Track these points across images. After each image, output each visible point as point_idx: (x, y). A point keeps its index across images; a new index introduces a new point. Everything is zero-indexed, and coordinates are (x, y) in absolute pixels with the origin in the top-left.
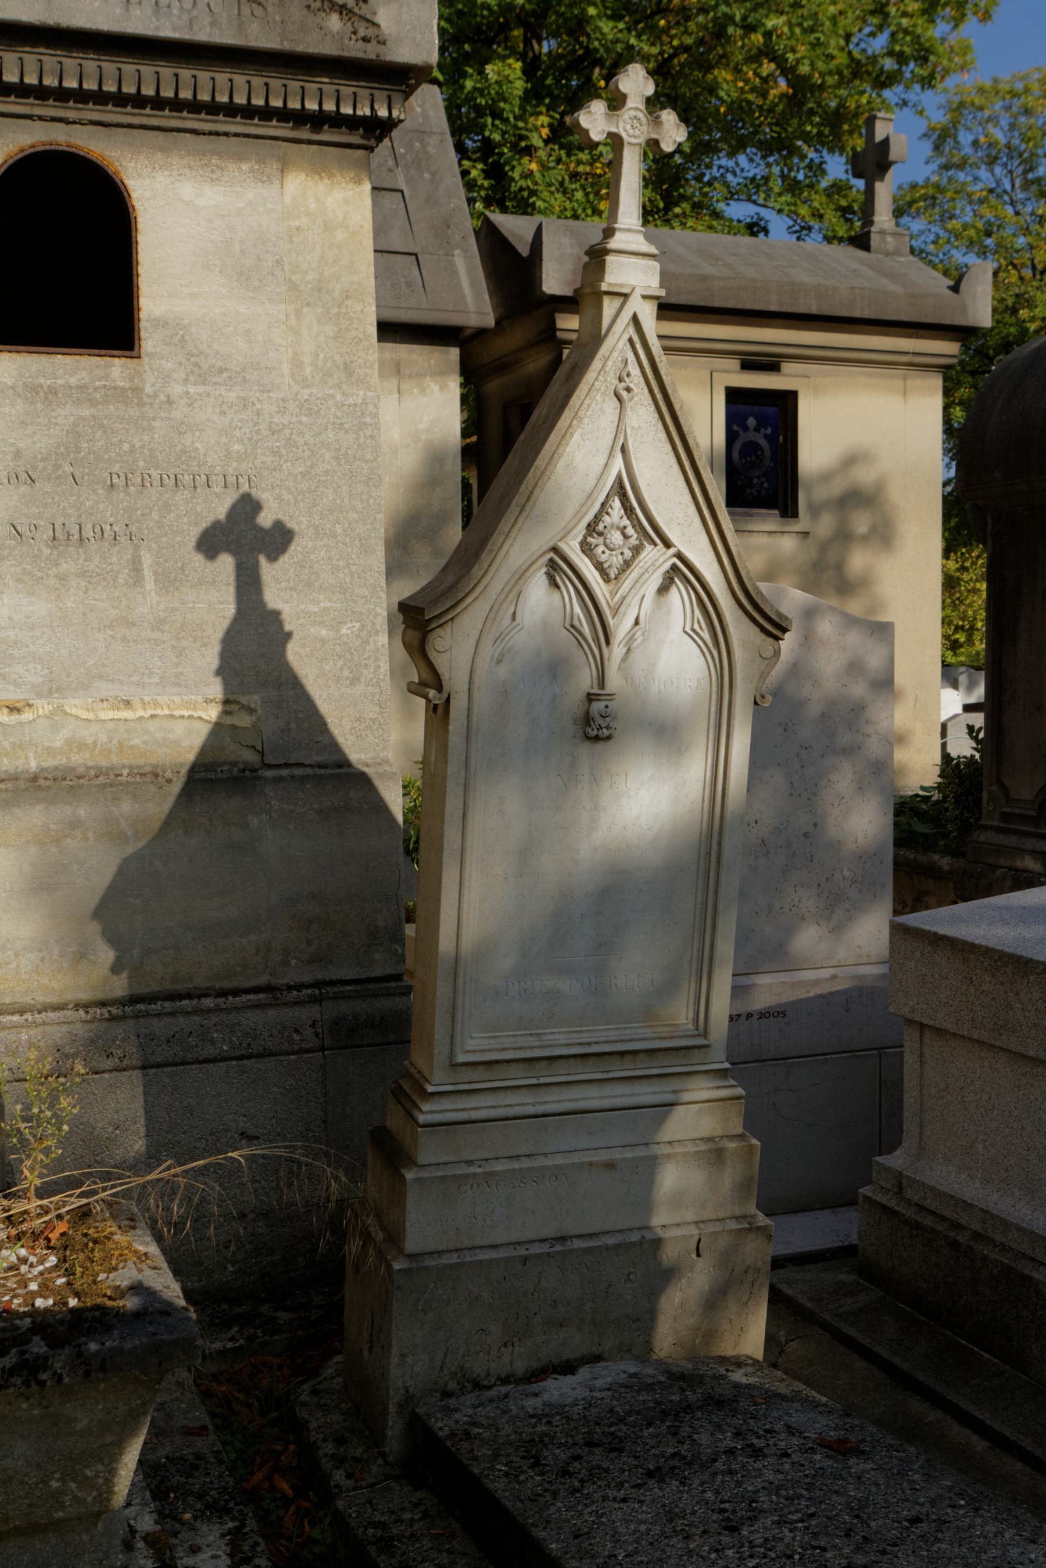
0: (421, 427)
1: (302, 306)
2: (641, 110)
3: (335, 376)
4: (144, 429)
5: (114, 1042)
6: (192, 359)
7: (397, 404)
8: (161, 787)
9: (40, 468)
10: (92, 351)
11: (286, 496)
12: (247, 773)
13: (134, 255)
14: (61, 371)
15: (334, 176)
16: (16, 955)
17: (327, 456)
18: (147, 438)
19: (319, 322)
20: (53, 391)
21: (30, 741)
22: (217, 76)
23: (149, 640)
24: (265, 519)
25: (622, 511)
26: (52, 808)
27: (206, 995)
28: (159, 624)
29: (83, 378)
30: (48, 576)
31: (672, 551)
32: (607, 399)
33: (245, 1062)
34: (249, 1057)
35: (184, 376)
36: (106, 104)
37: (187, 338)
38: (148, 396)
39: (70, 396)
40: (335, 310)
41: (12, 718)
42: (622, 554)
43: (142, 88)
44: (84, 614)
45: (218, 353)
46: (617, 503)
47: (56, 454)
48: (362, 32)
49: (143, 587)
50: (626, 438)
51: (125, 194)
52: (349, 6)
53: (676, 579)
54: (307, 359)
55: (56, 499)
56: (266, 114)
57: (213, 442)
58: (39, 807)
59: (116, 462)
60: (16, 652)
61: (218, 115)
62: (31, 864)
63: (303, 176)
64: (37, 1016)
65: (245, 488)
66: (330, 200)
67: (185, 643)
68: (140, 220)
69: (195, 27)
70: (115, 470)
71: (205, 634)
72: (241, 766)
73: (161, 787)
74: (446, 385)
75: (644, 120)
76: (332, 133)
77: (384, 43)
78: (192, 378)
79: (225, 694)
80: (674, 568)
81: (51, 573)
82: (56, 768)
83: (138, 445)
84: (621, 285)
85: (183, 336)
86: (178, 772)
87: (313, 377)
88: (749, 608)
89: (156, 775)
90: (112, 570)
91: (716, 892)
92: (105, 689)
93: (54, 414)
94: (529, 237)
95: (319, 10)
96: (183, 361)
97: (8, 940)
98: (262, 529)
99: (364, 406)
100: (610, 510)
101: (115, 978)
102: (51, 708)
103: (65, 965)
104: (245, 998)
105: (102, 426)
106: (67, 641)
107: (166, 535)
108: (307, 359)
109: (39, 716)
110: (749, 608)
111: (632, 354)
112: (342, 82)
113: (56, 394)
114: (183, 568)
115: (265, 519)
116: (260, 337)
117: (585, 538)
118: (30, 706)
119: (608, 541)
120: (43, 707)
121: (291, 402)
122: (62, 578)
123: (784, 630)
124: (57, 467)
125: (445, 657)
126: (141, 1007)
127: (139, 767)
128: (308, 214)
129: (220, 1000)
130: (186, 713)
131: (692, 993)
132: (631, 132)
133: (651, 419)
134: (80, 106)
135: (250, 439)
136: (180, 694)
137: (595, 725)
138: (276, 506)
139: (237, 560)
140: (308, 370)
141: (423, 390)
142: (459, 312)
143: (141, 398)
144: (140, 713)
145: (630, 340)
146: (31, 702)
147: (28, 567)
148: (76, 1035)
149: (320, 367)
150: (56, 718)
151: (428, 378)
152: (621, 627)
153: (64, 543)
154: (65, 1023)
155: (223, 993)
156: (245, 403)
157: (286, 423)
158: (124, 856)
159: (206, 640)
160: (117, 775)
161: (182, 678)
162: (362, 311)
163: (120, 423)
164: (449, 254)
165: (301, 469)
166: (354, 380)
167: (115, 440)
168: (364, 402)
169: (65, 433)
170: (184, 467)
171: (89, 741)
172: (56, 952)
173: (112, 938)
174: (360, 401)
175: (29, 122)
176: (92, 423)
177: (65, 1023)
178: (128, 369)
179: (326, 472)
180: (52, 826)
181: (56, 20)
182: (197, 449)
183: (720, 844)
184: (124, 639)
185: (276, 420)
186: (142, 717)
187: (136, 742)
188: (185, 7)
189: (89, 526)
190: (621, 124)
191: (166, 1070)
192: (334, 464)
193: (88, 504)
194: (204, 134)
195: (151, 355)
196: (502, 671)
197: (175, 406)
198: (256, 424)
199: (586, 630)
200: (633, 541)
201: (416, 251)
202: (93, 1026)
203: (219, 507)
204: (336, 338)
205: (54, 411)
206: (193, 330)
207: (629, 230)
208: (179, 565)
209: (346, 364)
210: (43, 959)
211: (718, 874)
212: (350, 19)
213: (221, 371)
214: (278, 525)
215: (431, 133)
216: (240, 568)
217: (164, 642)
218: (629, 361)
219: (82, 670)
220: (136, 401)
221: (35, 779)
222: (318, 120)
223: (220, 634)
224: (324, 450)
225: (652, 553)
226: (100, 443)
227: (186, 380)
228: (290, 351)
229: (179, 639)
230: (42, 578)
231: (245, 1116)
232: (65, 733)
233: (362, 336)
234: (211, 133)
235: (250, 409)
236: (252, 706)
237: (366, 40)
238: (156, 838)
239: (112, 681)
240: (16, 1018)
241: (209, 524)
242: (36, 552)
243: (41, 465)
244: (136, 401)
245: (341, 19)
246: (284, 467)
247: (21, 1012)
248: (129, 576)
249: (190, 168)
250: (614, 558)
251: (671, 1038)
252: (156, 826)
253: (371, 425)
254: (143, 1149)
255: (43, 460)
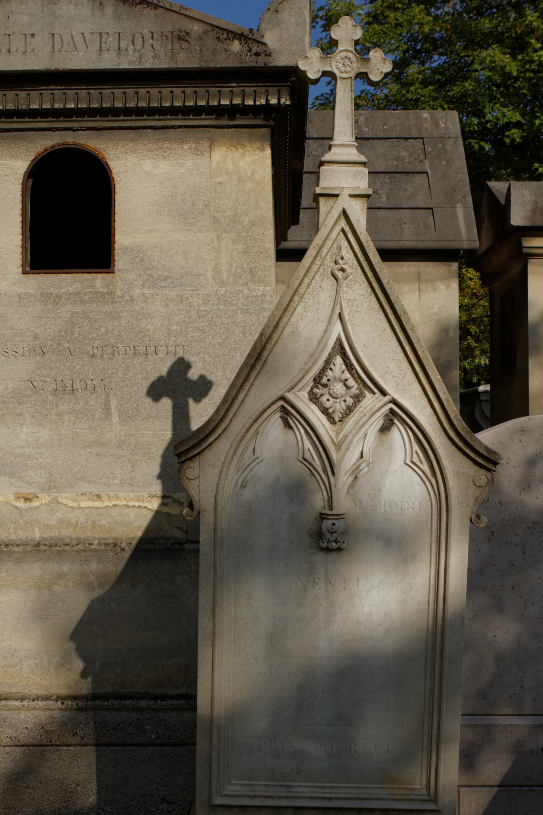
0: (433, 311)
1: (222, 233)
2: (350, 52)
3: (243, 278)
4: (115, 318)
5: (79, 725)
6: (148, 272)
7: (418, 298)
8: (117, 554)
9: (49, 345)
10: (83, 270)
11: (208, 359)
12: (176, 545)
13: (113, 209)
14: (64, 284)
15: (246, 147)
16: (21, 661)
17: (237, 332)
18: (116, 324)
19: (233, 243)
20: (59, 296)
21: (36, 520)
22: (163, 90)
23: (113, 455)
24: (193, 374)
25: (344, 367)
26: (46, 564)
27: (143, 698)
28: (121, 444)
29: (78, 288)
30: (51, 413)
31: (387, 398)
32: (325, 279)
33: (166, 748)
34: (169, 745)
35: (142, 283)
36: (96, 116)
37: (144, 258)
38: (118, 297)
39: (69, 299)
40: (244, 234)
41: (26, 505)
42: (345, 401)
43: (115, 103)
44: (73, 438)
45: (164, 267)
46: (339, 360)
47: (59, 336)
48: (255, 50)
49: (111, 420)
50: (341, 309)
51: (109, 171)
52: (245, 34)
53: (396, 421)
54: (224, 268)
55: (58, 365)
56: (197, 111)
57: (159, 324)
58: (38, 564)
59: (97, 340)
60: (29, 462)
61: (166, 115)
62: (32, 601)
63: (224, 149)
64: (31, 703)
65: (180, 354)
66: (242, 163)
67: (137, 458)
68: (117, 186)
69: (143, 60)
70: (95, 345)
71: (151, 451)
72: (173, 541)
73: (117, 554)
74: (449, 286)
75: (354, 58)
76: (243, 119)
77: (270, 55)
78: (147, 284)
79: (163, 491)
80: (392, 411)
81: (53, 411)
82: (52, 538)
83: (111, 328)
84: (333, 188)
85: (142, 258)
86: (130, 544)
87: (228, 279)
88: (460, 444)
89: (115, 545)
90: (91, 410)
91: (441, 678)
92: (84, 487)
93: (58, 311)
94: (505, 191)
95: (225, 39)
96: (142, 273)
97: (16, 650)
98: (191, 381)
99: (263, 297)
100: (332, 366)
101: (83, 681)
102: (50, 499)
103: (51, 670)
104: (169, 702)
105: (88, 317)
106: (62, 455)
107: (127, 386)
108: (224, 268)
109: (42, 504)
110: (460, 444)
111: (346, 242)
112: (245, 85)
113: (61, 299)
114: (137, 408)
115: (193, 374)
116: (193, 255)
117: (312, 389)
118: (37, 497)
119: (331, 391)
120: (45, 498)
121: (213, 296)
122: (60, 415)
123: (495, 464)
124: (59, 344)
125: (195, 483)
126: (98, 702)
127: (105, 539)
128: (227, 173)
129: (152, 702)
130: (137, 504)
131: (425, 763)
132: (343, 69)
133: (365, 292)
134: (80, 119)
135: (184, 322)
136: (133, 491)
137: (327, 537)
138: (200, 365)
139: (173, 402)
140: (225, 275)
141: (435, 289)
142: (456, 240)
143: (114, 298)
144: (107, 503)
145: (343, 230)
146: (38, 495)
147: (39, 408)
148: (55, 718)
149: (233, 272)
150: (53, 505)
151: (438, 281)
152: (347, 461)
153: (62, 392)
154: (48, 709)
155: (155, 698)
156: (181, 299)
157: (209, 310)
158: (92, 599)
159: (151, 455)
160: (90, 544)
161: (135, 480)
162: (263, 234)
163: (100, 315)
164: (453, 207)
165: (219, 341)
166: (256, 279)
167: (96, 326)
168: (264, 294)
169: (65, 322)
170: (140, 341)
171: (73, 521)
172: (45, 660)
173: (82, 653)
174: (261, 293)
175: (51, 132)
176: (82, 315)
177: (48, 709)
178: (106, 280)
179: (236, 342)
180: (46, 577)
181: (56, 67)
182: (149, 330)
183: (442, 640)
184: (98, 455)
185: (202, 309)
186: (107, 506)
187: (104, 522)
188: (137, 49)
189: (78, 381)
190: (334, 64)
191: (112, 748)
192: (241, 336)
193: (77, 367)
194: (159, 129)
195: (121, 271)
196: (247, 493)
197: (135, 302)
198: (188, 312)
199: (317, 463)
200: (354, 391)
201: (432, 207)
202: (66, 713)
203: (162, 367)
204: (244, 252)
205: (59, 309)
206: (149, 253)
207: (343, 145)
208: (135, 405)
209: (251, 269)
210: (37, 665)
211: (442, 666)
212: (246, 42)
213: (166, 278)
214: (202, 378)
215: (449, 138)
216: (175, 408)
217: (123, 457)
218: (343, 248)
219: (70, 474)
220: (110, 300)
221: (38, 545)
222: (232, 112)
223: (161, 452)
224: (234, 328)
225: (371, 401)
226: (87, 328)
227: (143, 286)
228: (213, 263)
229: (133, 455)
230: (47, 415)
231: (165, 786)
232: (58, 515)
233: (262, 250)
234: (163, 128)
235: (185, 302)
236: (181, 500)
237: (257, 54)
238: (112, 588)
239: (89, 482)
240: (17, 703)
241: (155, 378)
242: (44, 398)
243: (49, 343)
244: (110, 300)
245: (241, 44)
246: (207, 339)
247: (22, 699)
248: (102, 413)
249: (150, 150)
250: (338, 405)
251: (405, 800)
252: (113, 579)
253: (268, 309)
254: (95, 802)
255: (51, 340)
